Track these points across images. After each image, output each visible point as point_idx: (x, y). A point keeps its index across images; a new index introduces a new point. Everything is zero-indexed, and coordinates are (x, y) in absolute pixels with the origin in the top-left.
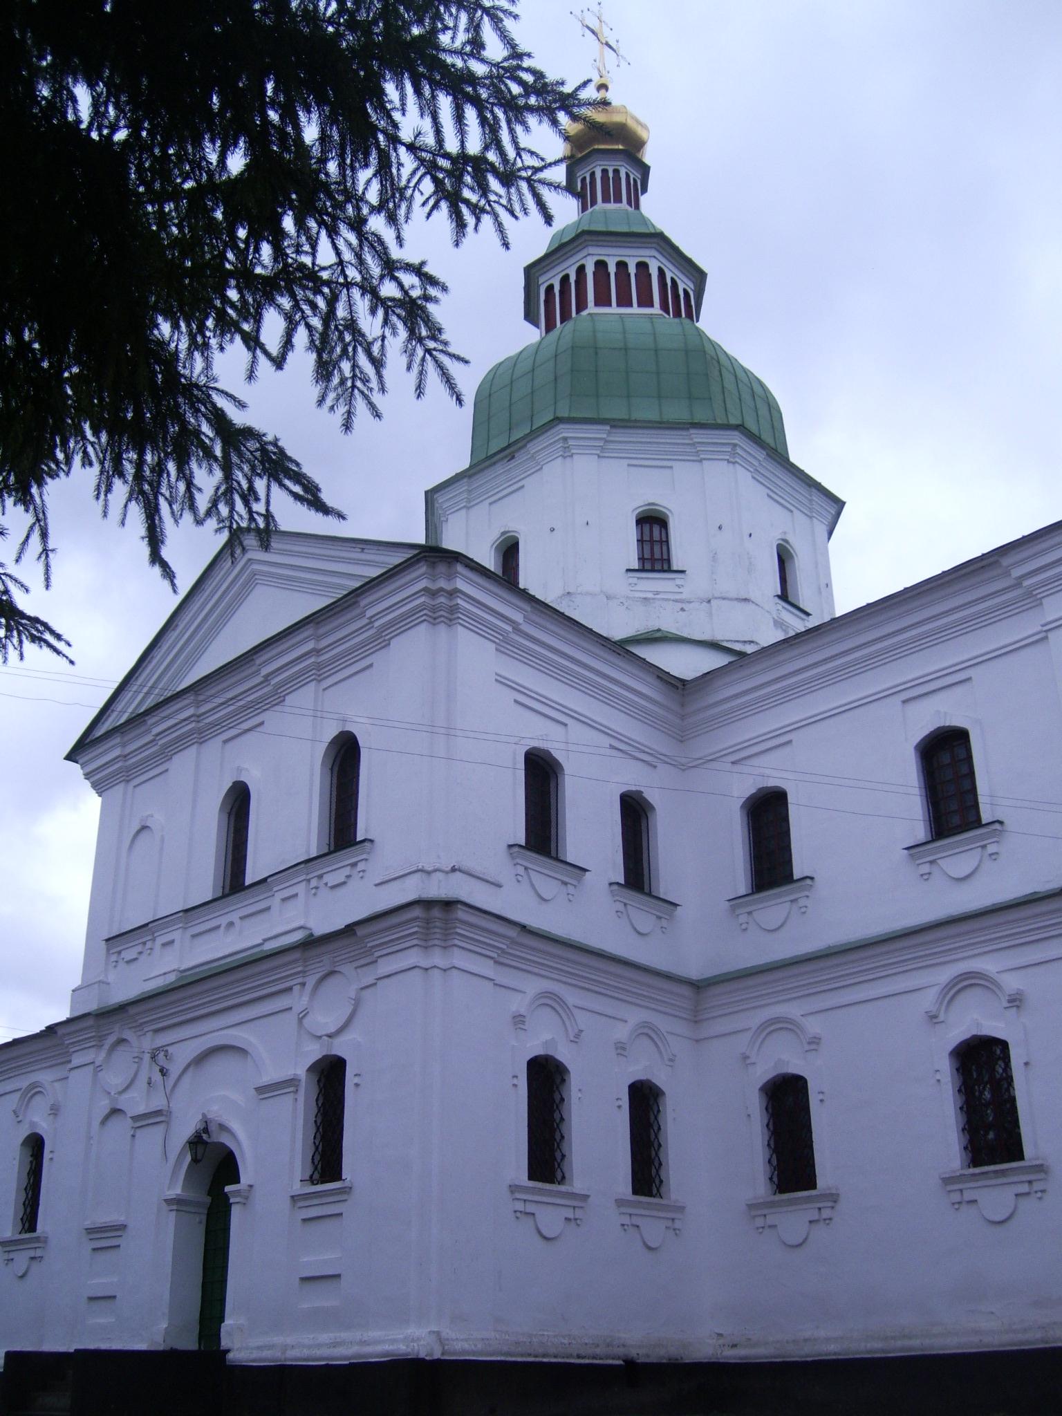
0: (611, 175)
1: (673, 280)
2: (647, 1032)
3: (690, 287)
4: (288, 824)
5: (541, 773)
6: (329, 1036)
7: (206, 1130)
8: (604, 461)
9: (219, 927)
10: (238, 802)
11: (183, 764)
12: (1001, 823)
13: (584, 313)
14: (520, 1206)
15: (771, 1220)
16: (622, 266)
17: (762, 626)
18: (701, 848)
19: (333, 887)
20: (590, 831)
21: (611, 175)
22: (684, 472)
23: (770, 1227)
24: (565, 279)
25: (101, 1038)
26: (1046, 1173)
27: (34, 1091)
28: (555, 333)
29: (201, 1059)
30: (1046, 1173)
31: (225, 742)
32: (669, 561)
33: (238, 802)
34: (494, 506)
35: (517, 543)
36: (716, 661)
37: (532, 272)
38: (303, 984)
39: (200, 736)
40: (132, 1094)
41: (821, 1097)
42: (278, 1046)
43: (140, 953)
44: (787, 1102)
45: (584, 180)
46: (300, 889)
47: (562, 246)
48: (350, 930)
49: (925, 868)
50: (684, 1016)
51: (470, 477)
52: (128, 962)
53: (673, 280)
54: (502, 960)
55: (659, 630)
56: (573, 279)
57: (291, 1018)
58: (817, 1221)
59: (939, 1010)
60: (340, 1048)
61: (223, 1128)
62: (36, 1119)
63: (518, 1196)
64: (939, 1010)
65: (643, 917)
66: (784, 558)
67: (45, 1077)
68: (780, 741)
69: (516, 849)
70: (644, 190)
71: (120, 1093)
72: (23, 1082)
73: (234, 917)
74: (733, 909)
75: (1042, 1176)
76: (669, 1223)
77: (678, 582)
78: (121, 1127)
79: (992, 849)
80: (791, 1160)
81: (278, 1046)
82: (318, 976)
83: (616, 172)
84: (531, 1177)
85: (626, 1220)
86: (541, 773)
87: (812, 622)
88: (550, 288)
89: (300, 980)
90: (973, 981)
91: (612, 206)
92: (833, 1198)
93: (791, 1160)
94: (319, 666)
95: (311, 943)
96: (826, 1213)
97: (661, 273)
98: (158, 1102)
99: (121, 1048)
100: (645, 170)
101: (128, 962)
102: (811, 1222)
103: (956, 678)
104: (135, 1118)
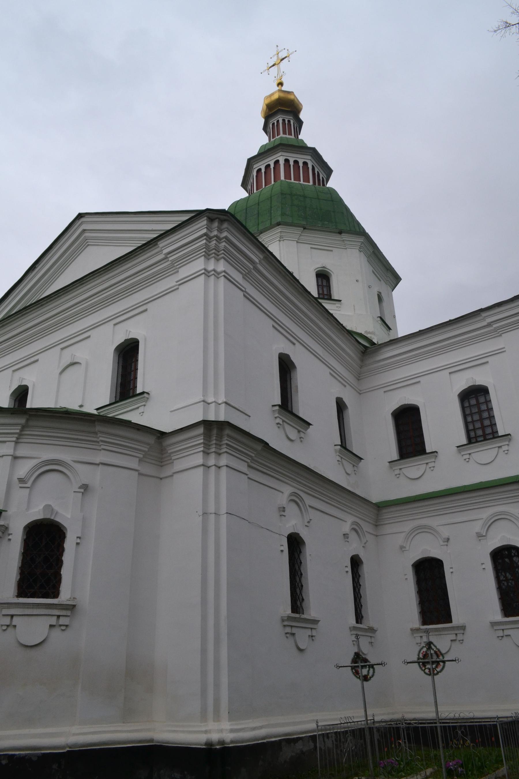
0: (287, 122)
8: (298, 244)
16: (296, 162)
21: (287, 122)
23: (507, 636)
24: (268, 166)
34: (65, 351)
37: (251, 162)
41: (451, 570)
45: (273, 124)
50: (371, 522)
58: (455, 640)
68: (413, 382)
74: (391, 468)
77: (337, 305)
83: (289, 121)
88: (259, 170)
90: (426, 530)
96: (460, 637)
102: (452, 640)
103: (480, 362)
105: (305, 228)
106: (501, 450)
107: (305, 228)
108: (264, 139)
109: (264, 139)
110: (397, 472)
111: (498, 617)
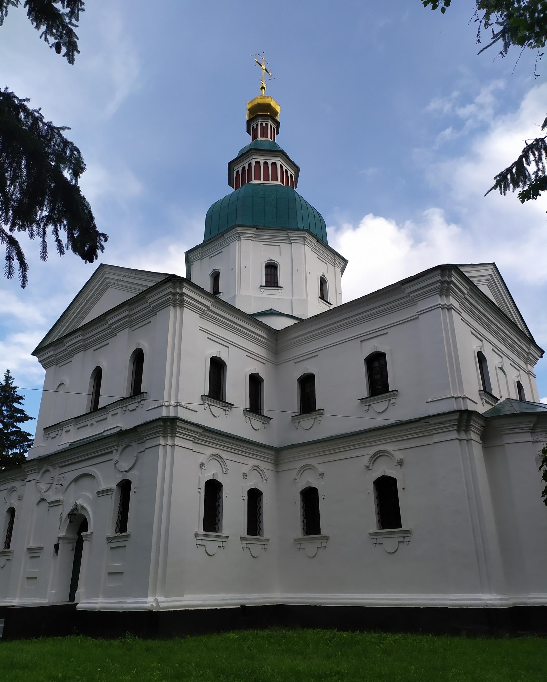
1: (286, 170)
2: (257, 468)
3: (293, 173)
4: (116, 385)
5: (217, 366)
6: (126, 471)
7: (76, 509)
9: (87, 425)
10: (98, 374)
11: (78, 358)
12: (397, 391)
13: (250, 183)
14: (199, 542)
15: (302, 546)
16: (266, 163)
17: (315, 308)
18: (281, 398)
19: (131, 411)
20: (237, 390)
21: (264, 125)
22: (285, 247)
24: (244, 168)
25: (40, 469)
26: (410, 534)
27: (13, 489)
28: (238, 190)
29: (77, 479)
30: (410, 534)
31: (94, 350)
32: (277, 282)
33: (98, 374)
35: (219, 274)
36: (291, 322)
37: (231, 165)
38: (117, 450)
39: (85, 348)
40: (50, 493)
41: (323, 497)
42: (107, 477)
43: (57, 435)
44: (310, 497)
46: (119, 411)
47: (243, 154)
48: (135, 429)
49: (367, 408)
51: (202, 247)
52: (52, 438)
53: (286, 170)
54: (196, 441)
55: (272, 309)
56: (247, 168)
57: (112, 463)
59: (370, 464)
60: (129, 476)
61: (83, 508)
62: (13, 502)
63: (198, 538)
64: (370, 464)
65: (257, 423)
66: (323, 282)
67: (17, 484)
68: (312, 355)
69: (204, 397)
70: (277, 133)
71: (45, 492)
72: (9, 486)
73: (93, 421)
75: (409, 535)
76: (263, 546)
78: (44, 505)
79: (392, 401)
80: (311, 523)
81: (107, 477)
82: (123, 447)
83: (266, 124)
84: (204, 530)
85: (244, 546)
86: (217, 366)
87: (332, 307)
89: (116, 448)
91: (264, 139)
92: (327, 538)
93: (311, 523)
94: (131, 322)
95: (122, 434)
97: (281, 167)
98: (60, 497)
99: (47, 473)
100: (278, 124)
101: (52, 438)
103: (381, 333)
104: (49, 503)
105: (257, 229)
106: (316, 420)
107: (257, 229)
108: (246, 140)
109: (246, 140)
110: (367, 408)
111: (201, 531)
